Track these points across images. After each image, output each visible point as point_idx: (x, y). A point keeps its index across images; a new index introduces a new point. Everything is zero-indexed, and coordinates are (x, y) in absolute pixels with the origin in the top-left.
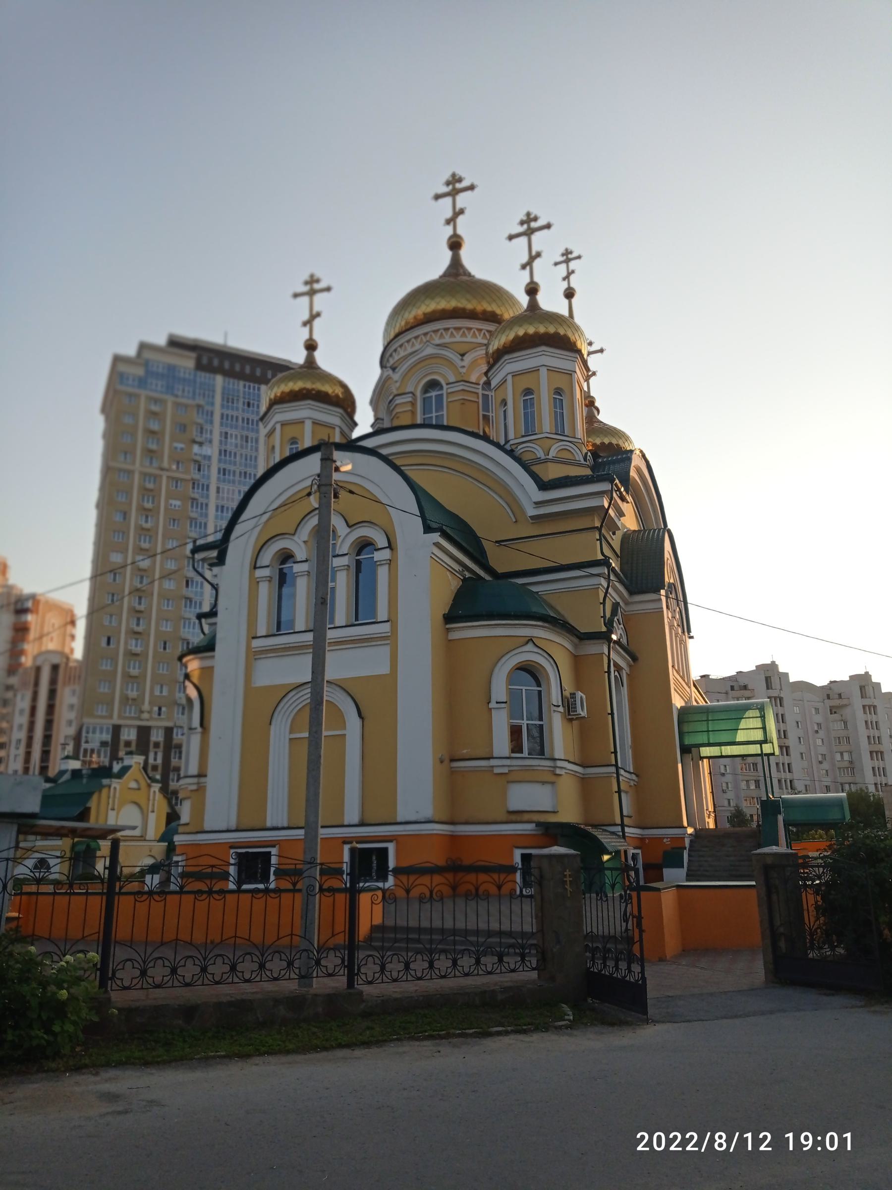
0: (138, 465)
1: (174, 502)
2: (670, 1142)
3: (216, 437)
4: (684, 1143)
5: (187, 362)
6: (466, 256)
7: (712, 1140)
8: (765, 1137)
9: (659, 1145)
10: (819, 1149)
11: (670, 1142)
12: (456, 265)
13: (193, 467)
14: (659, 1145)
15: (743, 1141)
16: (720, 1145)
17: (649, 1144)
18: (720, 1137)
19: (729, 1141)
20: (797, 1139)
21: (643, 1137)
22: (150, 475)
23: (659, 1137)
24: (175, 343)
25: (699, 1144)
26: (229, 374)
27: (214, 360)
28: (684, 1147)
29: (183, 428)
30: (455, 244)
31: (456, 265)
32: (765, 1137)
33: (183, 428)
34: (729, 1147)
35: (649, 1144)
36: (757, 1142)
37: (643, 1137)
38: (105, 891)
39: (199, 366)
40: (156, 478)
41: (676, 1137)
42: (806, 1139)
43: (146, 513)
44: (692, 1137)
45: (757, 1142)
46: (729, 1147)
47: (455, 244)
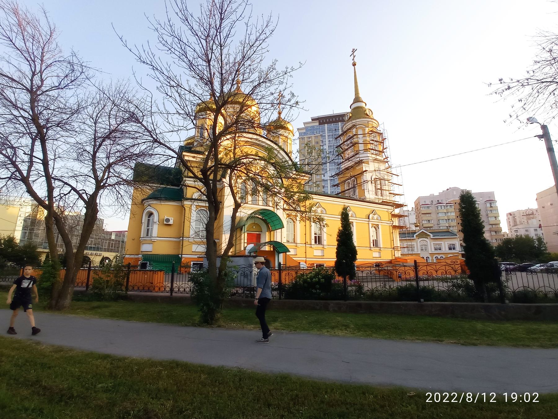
3: (327, 143)
5: (317, 124)
8: (493, 395)
9: (437, 399)
12: (279, 117)
14: (437, 399)
16: (469, 399)
17: (432, 398)
21: (429, 395)
24: (313, 120)
26: (327, 123)
28: (450, 401)
31: (279, 117)
32: (493, 395)
34: (474, 399)
35: (432, 398)
37: (429, 395)
38: (174, 294)
39: (320, 124)
41: (446, 395)
42: (514, 396)
44: (454, 395)
46: (474, 399)
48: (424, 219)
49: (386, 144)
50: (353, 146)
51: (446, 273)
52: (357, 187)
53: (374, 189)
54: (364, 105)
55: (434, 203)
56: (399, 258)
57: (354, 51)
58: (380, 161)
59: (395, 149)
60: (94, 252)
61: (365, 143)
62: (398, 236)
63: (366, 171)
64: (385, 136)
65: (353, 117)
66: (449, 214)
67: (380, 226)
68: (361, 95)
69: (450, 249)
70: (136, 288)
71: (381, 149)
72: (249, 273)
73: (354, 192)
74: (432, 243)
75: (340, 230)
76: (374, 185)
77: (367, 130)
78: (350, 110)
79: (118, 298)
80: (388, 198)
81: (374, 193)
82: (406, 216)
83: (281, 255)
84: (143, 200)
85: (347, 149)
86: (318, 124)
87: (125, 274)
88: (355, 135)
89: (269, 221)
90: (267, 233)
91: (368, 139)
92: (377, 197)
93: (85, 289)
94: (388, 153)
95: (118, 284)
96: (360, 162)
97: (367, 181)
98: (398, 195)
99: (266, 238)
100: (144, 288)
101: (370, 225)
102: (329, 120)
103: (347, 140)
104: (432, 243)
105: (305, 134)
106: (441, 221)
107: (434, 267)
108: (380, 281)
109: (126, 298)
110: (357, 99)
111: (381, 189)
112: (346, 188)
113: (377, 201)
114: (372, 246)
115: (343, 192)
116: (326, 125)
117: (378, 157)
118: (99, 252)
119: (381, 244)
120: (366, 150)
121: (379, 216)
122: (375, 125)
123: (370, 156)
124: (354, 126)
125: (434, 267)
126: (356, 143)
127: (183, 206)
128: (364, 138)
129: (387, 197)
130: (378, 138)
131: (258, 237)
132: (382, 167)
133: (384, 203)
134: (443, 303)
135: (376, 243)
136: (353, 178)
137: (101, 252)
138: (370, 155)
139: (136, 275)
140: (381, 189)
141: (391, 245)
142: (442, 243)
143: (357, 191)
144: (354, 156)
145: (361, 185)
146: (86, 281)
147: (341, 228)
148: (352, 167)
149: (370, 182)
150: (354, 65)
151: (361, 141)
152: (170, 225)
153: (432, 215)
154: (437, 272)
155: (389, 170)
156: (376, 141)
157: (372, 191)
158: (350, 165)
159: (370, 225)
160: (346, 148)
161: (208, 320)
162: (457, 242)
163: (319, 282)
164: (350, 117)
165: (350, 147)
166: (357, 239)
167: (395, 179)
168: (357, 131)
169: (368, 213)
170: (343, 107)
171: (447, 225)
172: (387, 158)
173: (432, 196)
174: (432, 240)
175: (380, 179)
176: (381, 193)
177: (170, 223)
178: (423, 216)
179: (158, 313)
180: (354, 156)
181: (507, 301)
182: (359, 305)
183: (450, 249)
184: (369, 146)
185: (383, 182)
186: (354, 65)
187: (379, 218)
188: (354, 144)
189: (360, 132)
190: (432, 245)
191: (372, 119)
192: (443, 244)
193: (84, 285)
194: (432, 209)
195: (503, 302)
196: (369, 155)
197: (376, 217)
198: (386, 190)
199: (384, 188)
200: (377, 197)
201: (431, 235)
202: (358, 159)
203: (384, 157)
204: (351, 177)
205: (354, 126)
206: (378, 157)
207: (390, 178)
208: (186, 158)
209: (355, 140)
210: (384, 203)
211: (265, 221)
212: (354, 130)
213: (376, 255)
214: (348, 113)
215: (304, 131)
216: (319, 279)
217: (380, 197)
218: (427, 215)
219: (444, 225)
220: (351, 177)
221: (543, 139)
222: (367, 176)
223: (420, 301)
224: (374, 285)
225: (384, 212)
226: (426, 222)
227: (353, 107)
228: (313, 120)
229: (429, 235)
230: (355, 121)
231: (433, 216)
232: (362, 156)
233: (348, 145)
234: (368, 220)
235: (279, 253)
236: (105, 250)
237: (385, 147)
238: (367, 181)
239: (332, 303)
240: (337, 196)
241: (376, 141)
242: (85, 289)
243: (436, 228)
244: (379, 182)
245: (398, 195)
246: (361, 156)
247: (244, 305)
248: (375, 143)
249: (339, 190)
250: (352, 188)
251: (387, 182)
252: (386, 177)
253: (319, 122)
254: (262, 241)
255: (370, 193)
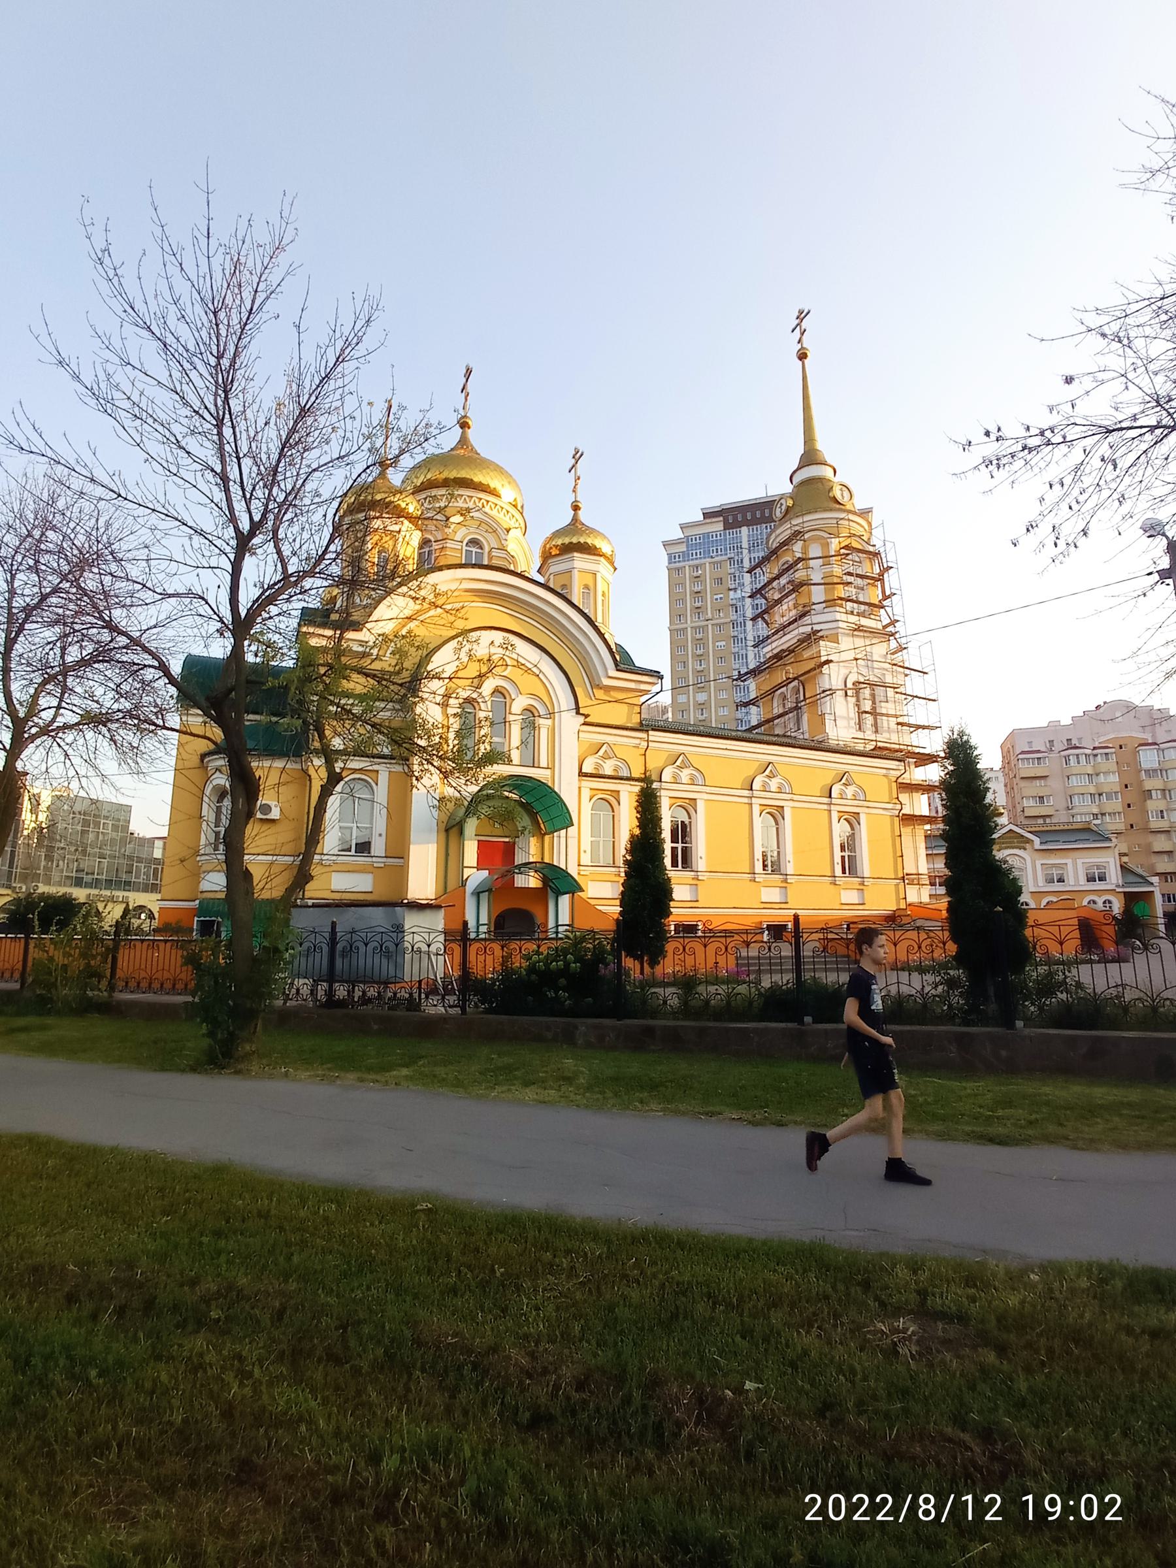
0: (690, 622)
1: (719, 644)
2: (853, 1509)
4: (874, 1509)
5: (717, 526)
6: (582, 515)
7: (914, 1506)
9: (837, 1512)
10: (1072, 1518)
11: (853, 1509)
13: (731, 611)
14: (837, 1512)
15: (960, 1507)
16: (927, 1513)
17: (823, 1511)
18: (927, 1501)
19: (939, 1509)
20: (1038, 1504)
22: (699, 627)
23: (837, 1501)
25: (895, 1511)
27: (734, 517)
29: (720, 581)
30: (576, 508)
33: (720, 581)
35: (823, 1511)
36: (981, 1508)
40: (705, 628)
42: (1053, 1503)
43: (700, 658)
45: (981, 1508)
47: (576, 508)
48: (1026, 792)
49: (891, 579)
50: (793, 590)
51: (920, 947)
52: (805, 709)
53: (853, 714)
54: (828, 473)
55: (1058, 746)
56: (921, 906)
57: (802, 316)
58: (873, 632)
59: (914, 597)
60: (107, 893)
61: (828, 584)
62: (923, 845)
63: (828, 662)
64: (890, 558)
65: (797, 509)
66: (1102, 778)
67: (863, 818)
68: (820, 445)
69: (1091, 879)
70: (132, 984)
71: (875, 595)
72: (392, 947)
73: (798, 721)
74: (1038, 863)
75: (632, 836)
76: (852, 700)
77: (834, 545)
78: (788, 488)
79: (86, 1008)
80: (894, 738)
81: (852, 723)
82: (648, 804)
83: (565, 900)
84: (203, 756)
85: (779, 602)
86: (720, 527)
87: (108, 949)
88: (800, 560)
89: (537, 807)
90: (533, 841)
91: (837, 570)
92: (860, 735)
93: (17, 986)
94: (896, 607)
95: (93, 974)
96: (812, 638)
97: (831, 692)
98: (924, 727)
99: (530, 850)
100: (174, 985)
101: (835, 816)
102: (754, 515)
103: (780, 574)
104: (1038, 863)
105: (685, 556)
106: (1076, 799)
107: (1055, 930)
108: (838, 970)
109: (108, 1009)
110: (810, 457)
111: (874, 713)
112: (777, 711)
113: (860, 747)
114: (838, 871)
115: (768, 721)
116: (744, 530)
117: (864, 622)
118: (120, 894)
119: (866, 867)
120: (831, 603)
121: (860, 788)
122: (858, 530)
123: (843, 618)
124: (797, 535)
125: (1055, 930)
126: (802, 584)
127: (305, 772)
128: (827, 569)
129: (891, 736)
130: (868, 566)
131: (509, 850)
132: (879, 650)
133: (879, 753)
134: (1094, 1033)
135: (773, 866)
136: (795, 683)
137: (126, 894)
138: (843, 617)
139: (1154, 959)
140: (874, 713)
141: (896, 871)
142: (1069, 861)
143: (805, 718)
144: (795, 620)
145: (815, 702)
146: (20, 966)
147: (637, 832)
148: (790, 651)
149: (842, 693)
150: (802, 356)
151: (816, 577)
152: (273, 821)
153: (1049, 782)
154: (1061, 944)
155: (898, 658)
156: (858, 576)
157: (848, 719)
158: (784, 647)
159: (835, 816)
160: (777, 596)
161: (221, 1057)
162: (1111, 861)
163: (565, 972)
164: (788, 509)
165: (787, 595)
166: (794, 853)
167: (914, 684)
168: (805, 550)
169: (829, 782)
170: (773, 481)
171: (1095, 811)
172: (893, 623)
173: (1054, 726)
174: (1036, 855)
175: (872, 685)
176: (875, 725)
177: (272, 816)
178: (1023, 784)
179: (155, 1042)
180: (795, 620)
181: (1019, 1024)
182: (649, 1031)
183: (1091, 879)
184: (841, 591)
185: (879, 691)
186: (802, 356)
187: (862, 796)
188: (798, 587)
189: (815, 551)
190: (1039, 867)
191: (850, 512)
192: (1070, 866)
193: (17, 975)
194: (1051, 765)
195: (1011, 1026)
196: (838, 616)
197: (850, 791)
198: (887, 715)
199: (884, 708)
200: (860, 735)
201: (1037, 840)
202: (808, 629)
203: (886, 621)
204: (789, 680)
205: (797, 535)
206: (864, 622)
207: (900, 679)
208: (313, 642)
209: (800, 575)
210: (879, 753)
211: (527, 807)
212: (798, 547)
213: (851, 897)
214: (782, 496)
215: (683, 548)
216: (567, 964)
217: (870, 735)
218: (1038, 782)
219: (1084, 810)
220: (789, 680)
221: (1170, 581)
222: (833, 676)
223: (802, 1022)
224: (776, 978)
225: (875, 776)
226: (1031, 803)
227: (796, 480)
228: (706, 515)
229: (1029, 841)
230: (799, 520)
231: (1055, 784)
232: (817, 619)
233: (781, 589)
234: (826, 800)
235: (558, 893)
236: (136, 887)
237: (888, 593)
238: (831, 692)
239: (583, 1025)
240: (749, 735)
241: (858, 576)
242: (17, 986)
243: (1061, 818)
244: (867, 692)
245: (924, 727)
246: (816, 619)
247: (376, 1027)
248: (859, 581)
249: (755, 715)
250: (791, 711)
251: (890, 692)
252: (889, 679)
253: (726, 522)
254: (519, 859)
255: (841, 723)
